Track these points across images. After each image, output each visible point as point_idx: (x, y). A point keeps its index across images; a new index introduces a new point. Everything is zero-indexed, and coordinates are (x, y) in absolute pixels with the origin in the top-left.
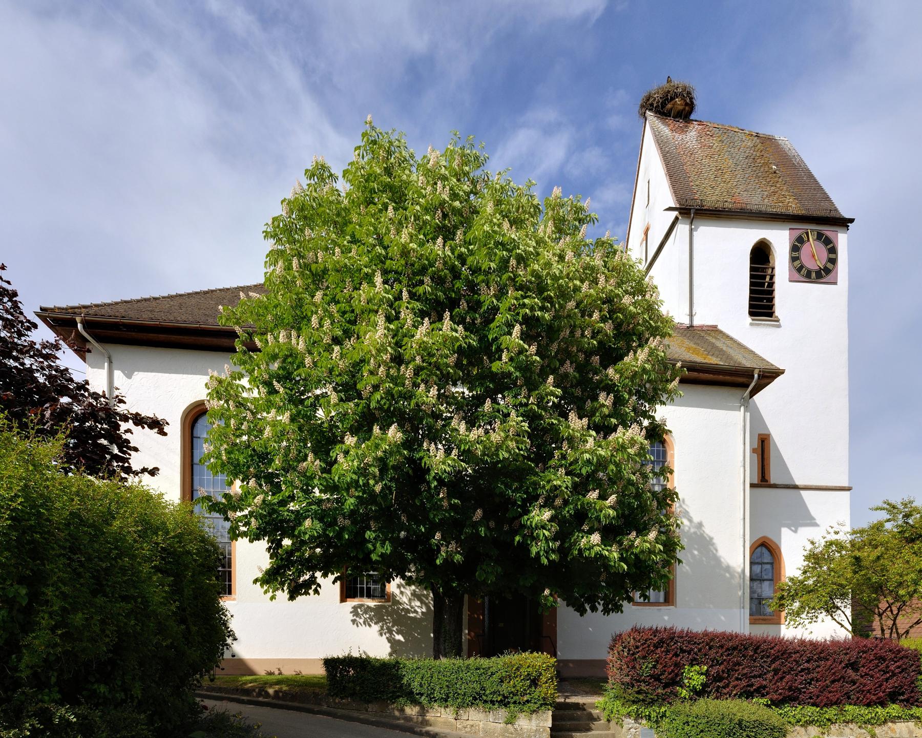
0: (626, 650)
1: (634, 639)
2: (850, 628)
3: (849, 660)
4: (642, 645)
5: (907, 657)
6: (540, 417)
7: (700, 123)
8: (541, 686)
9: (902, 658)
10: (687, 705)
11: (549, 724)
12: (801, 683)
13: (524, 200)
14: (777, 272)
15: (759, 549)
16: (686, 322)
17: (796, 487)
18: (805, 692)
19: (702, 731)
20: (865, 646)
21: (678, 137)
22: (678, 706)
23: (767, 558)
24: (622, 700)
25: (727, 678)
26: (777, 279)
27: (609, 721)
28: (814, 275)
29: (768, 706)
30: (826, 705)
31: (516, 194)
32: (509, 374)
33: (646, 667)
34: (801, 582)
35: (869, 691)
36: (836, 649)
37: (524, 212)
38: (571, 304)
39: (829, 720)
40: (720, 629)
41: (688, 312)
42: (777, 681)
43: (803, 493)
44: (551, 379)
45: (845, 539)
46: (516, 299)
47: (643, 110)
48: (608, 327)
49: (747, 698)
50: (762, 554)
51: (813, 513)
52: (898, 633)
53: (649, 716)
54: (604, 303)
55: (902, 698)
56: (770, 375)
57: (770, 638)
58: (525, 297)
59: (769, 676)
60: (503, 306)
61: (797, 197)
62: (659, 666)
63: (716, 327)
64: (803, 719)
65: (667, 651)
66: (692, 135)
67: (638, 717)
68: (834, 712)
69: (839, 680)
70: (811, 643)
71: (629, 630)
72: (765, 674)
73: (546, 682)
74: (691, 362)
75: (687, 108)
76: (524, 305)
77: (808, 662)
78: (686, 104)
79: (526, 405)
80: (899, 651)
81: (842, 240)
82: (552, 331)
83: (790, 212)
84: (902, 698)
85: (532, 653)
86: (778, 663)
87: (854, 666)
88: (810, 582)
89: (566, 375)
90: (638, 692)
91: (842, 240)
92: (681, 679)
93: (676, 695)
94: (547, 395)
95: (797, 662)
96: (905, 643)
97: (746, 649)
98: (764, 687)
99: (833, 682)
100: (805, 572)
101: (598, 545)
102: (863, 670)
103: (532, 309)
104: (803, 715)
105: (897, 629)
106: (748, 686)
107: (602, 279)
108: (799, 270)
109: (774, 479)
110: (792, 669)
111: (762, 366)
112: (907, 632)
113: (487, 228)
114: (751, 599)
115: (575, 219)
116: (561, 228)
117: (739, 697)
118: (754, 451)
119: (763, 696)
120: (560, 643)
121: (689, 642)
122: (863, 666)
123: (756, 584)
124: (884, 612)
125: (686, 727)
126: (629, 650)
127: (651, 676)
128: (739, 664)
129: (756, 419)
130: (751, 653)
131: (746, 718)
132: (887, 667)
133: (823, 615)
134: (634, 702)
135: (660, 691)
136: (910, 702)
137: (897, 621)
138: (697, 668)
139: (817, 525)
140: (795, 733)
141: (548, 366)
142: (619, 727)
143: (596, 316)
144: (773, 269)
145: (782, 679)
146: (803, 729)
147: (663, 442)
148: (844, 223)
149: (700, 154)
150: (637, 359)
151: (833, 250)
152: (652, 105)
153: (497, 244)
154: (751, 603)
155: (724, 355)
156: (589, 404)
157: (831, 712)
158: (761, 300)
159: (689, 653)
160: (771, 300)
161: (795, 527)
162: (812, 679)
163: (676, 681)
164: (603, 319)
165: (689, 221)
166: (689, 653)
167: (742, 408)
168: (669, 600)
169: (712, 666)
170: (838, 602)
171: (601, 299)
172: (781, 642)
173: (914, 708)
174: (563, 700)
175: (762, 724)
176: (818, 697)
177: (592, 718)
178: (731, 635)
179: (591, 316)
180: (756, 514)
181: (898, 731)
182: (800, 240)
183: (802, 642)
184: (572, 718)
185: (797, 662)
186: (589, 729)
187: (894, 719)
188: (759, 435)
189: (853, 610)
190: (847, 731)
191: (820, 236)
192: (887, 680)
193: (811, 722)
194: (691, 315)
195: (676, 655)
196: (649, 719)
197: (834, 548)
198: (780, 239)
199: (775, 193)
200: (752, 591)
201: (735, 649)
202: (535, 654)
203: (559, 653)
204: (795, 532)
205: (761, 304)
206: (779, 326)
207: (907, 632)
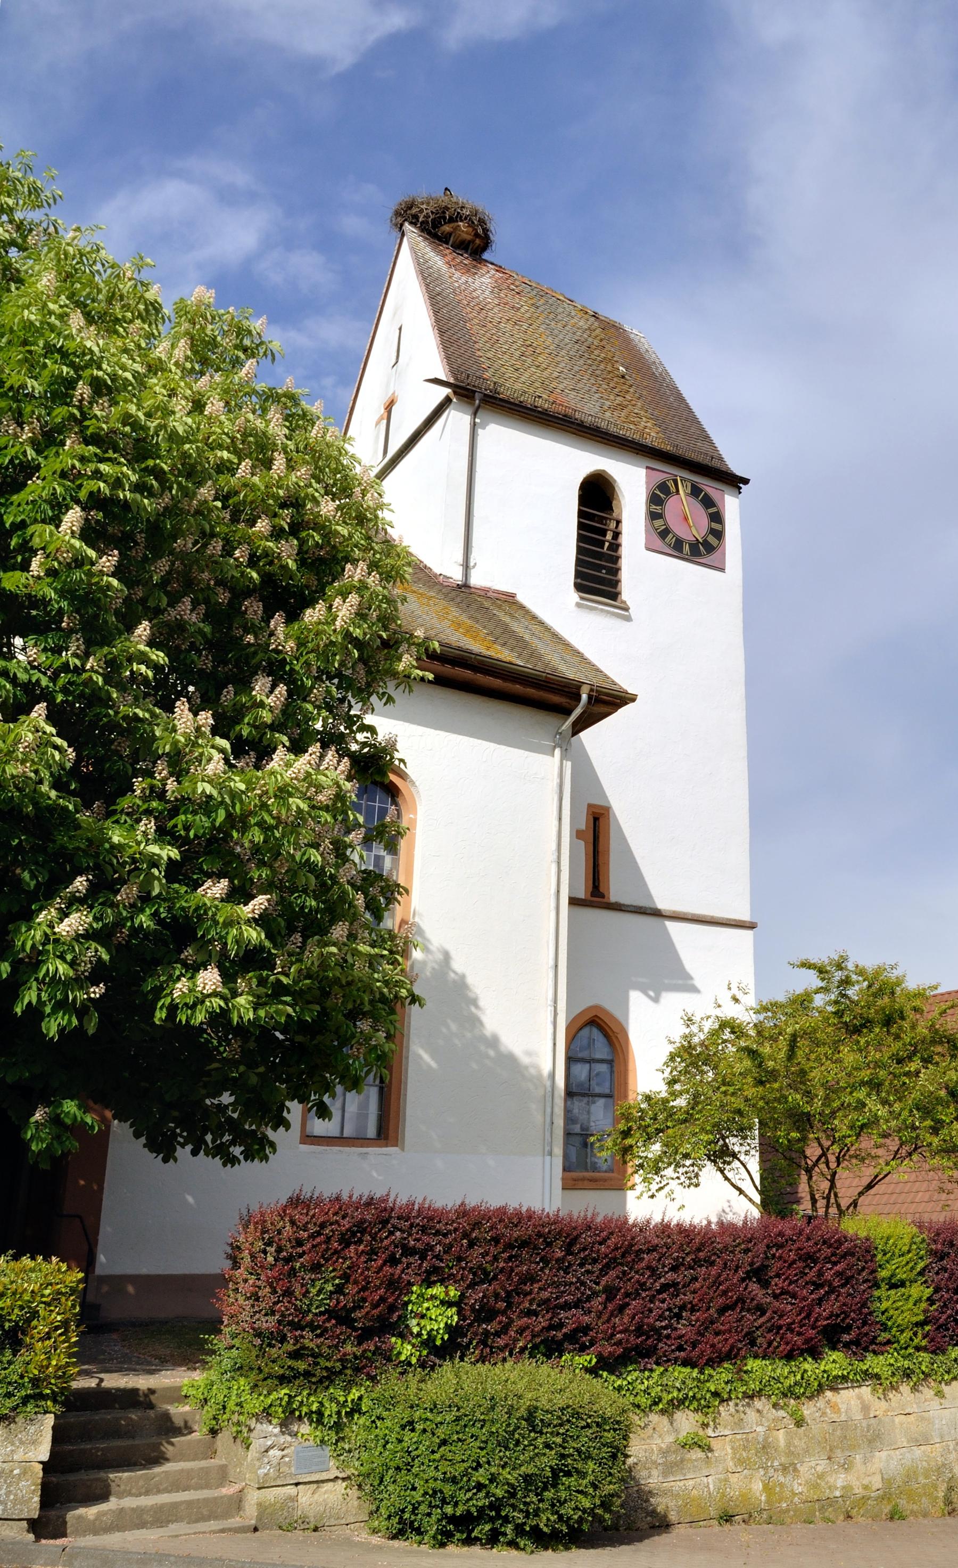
0: (271, 1250)
1: (293, 1223)
2: (757, 1198)
3: (751, 1264)
4: (312, 1237)
5: (853, 1255)
6: (106, 701)
7: (499, 269)
8: (30, 1347)
9: (844, 1256)
10: (412, 1380)
11: (43, 1452)
12: (661, 1317)
13: (126, 287)
14: (625, 528)
15: (586, 1031)
16: (456, 575)
17: (657, 913)
18: (668, 1337)
19: (444, 1442)
20: (781, 1234)
21: (460, 278)
22: (392, 1383)
23: (601, 1050)
24: (253, 1376)
25: (504, 1312)
26: (624, 540)
27: (214, 1432)
28: (686, 548)
29: (592, 1371)
30: (711, 1363)
31: (109, 271)
32: (45, 602)
33: (319, 1292)
34: (665, 1101)
35: (789, 1328)
36: (728, 1240)
37: (126, 307)
38: (205, 492)
39: (716, 1394)
40: (494, 1201)
41: (460, 559)
42: (612, 1314)
43: (671, 926)
44: (143, 629)
45: (747, 1019)
46: (82, 459)
47: (400, 220)
48: (287, 552)
49: (549, 1357)
50: (591, 1042)
51: (689, 966)
52: (839, 1206)
53: (320, 1413)
54: (283, 506)
55: (846, 1338)
56: (609, 701)
57: (599, 1219)
58: (101, 460)
59: (597, 1303)
60: (51, 464)
61: (659, 423)
62: (351, 1289)
63: (513, 596)
64: (666, 1397)
65: (372, 1253)
66: (482, 283)
67: (290, 1417)
68: (725, 1376)
69: (732, 1307)
70: (680, 1228)
71: (284, 1201)
72: (589, 1299)
73: (48, 1336)
74: (460, 649)
75: (478, 241)
76: (97, 475)
77: (674, 1269)
78: (477, 235)
79: (78, 671)
80: (840, 1242)
81: (731, 505)
82: (158, 535)
83: (648, 441)
84: (846, 1338)
85: (16, 1258)
86: (613, 1273)
87: (759, 1274)
88: (681, 1102)
89: (180, 626)
90: (296, 1355)
91: (731, 505)
92: (403, 1318)
93: (388, 1356)
94: (130, 660)
95: (653, 1270)
96: (852, 1226)
97: (549, 1245)
98: (586, 1329)
99: (722, 1311)
100: (671, 1082)
101: (215, 994)
102: (778, 1284)
103: (117, 483)
104: (666, 1388)
105: (836, 1195)
106: (551, 1327)
107: (279, 462)
108: (664, 533)
109: (616, 893)
110: (642, 1285)
111: (596, 682)
112: (855, 1204)
113: (32, 315)
114: (568, 1134)
115: (236, 347)
116: (204, 354)
117: (532, 1356)
118: (578, 835)
119: (583, 1349)
120: (106, 1230)
121: (424, 1230)
122: (778, 1276)
123: (578, 1105)
124: (816, 1164)
125: (408, 1436)
126: (279, 1250)
127: (330, 1313)
128: (531, 1278)
129: (584, 776)
130: (559, 1254)
131: (544, 1403)
132: (820, 1274)
133: (709, 1173)
134: (283, 1380)
135: (349, 1348)
136: (862, 1345)
137: (838, 1184)
138: (438, 1290)
139: (694, 990)
140: (649, 1430)
141: (143, 601)
142: (239, 1449)
143: (262, 525)
144: (618, 522)
145: (621, 1309)
146: (665, 1420)
147: (393, 792)
148: (735, 482)
149: (496, 313)
150: (333, 615)
151: (717, 518)
152: (415, 217)
153: (50, 349)
154: (566, 1144)
155: (525, 648)
156: (228, 695)
157: (720, 1377)
158: (599, 568)
159: (423, 1258)
160: (616, 571)
161: (655, 991)
162: (682, 1308)
163: (390, 1322)
164: (277, 534)
165: (471, 410)
166: (423, 1258)
167: (557, 752)
168: (387, 1130)
169: (472, 1286)
170: (734, 1143)
171: (275, 497)
172: (621, 1226)
173: (869, 1356)
174: (92, 1383)
175: (577, 1415)
176: (694, 1345)
177: (170, 1428)
178: (518, 1214)
179: (252, 523)
180: (580, 960)
181: (843, 1408)
182: (663, 487)
183: (664, 1228)
184: (115, 1432)
185: (653, 1270)
186: (158, 1459)
187: (835, 1383)
188: (590, 806)
189: (762, 1161)
190: (751, 1415)
191: (695, 491)
192: (820, 1301)
193: (682, 1402)
194: (466, 567)
195: (393, 1261)
196: (320, 1422)
197: (727, 1035)
198: (632, 482)
199: (622, 407)
200: (569, 1118)
201: (524, 1244)
202: (26, 1261)
203: (102, 1258)
204: (656, 1000)
205: (597, 573)
206: (628, 619)
207: (855, 1204)
